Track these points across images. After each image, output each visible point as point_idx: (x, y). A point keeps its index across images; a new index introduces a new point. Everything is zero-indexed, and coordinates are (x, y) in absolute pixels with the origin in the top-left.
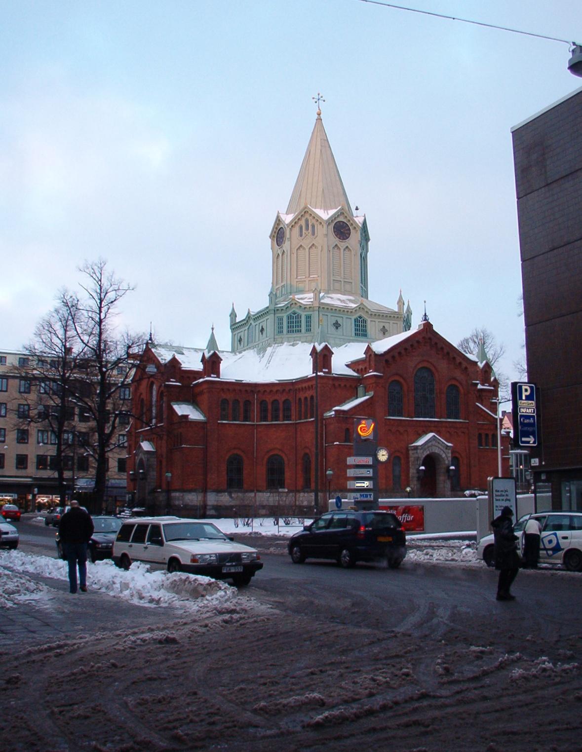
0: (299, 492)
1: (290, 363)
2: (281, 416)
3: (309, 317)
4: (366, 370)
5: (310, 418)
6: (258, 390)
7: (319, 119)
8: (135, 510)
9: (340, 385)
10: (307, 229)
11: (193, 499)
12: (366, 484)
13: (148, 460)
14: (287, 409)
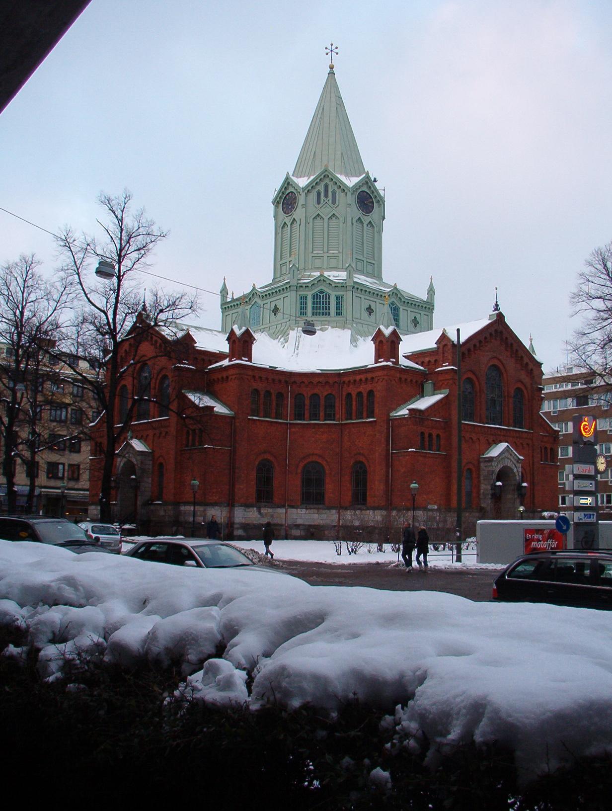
0: (346, 509)
1: (337, 350)
2: (322, 414)
3: (339, 299)
4: (437, 363)
5: (368, 417)
6: (293, 380)
7: (332, 73)
8: (127, 526)
9: (406, 379)
10: (326, 196)
11: (218, 514)
12: (588, 501)
13: (142, 463)
14: (330, 406)
